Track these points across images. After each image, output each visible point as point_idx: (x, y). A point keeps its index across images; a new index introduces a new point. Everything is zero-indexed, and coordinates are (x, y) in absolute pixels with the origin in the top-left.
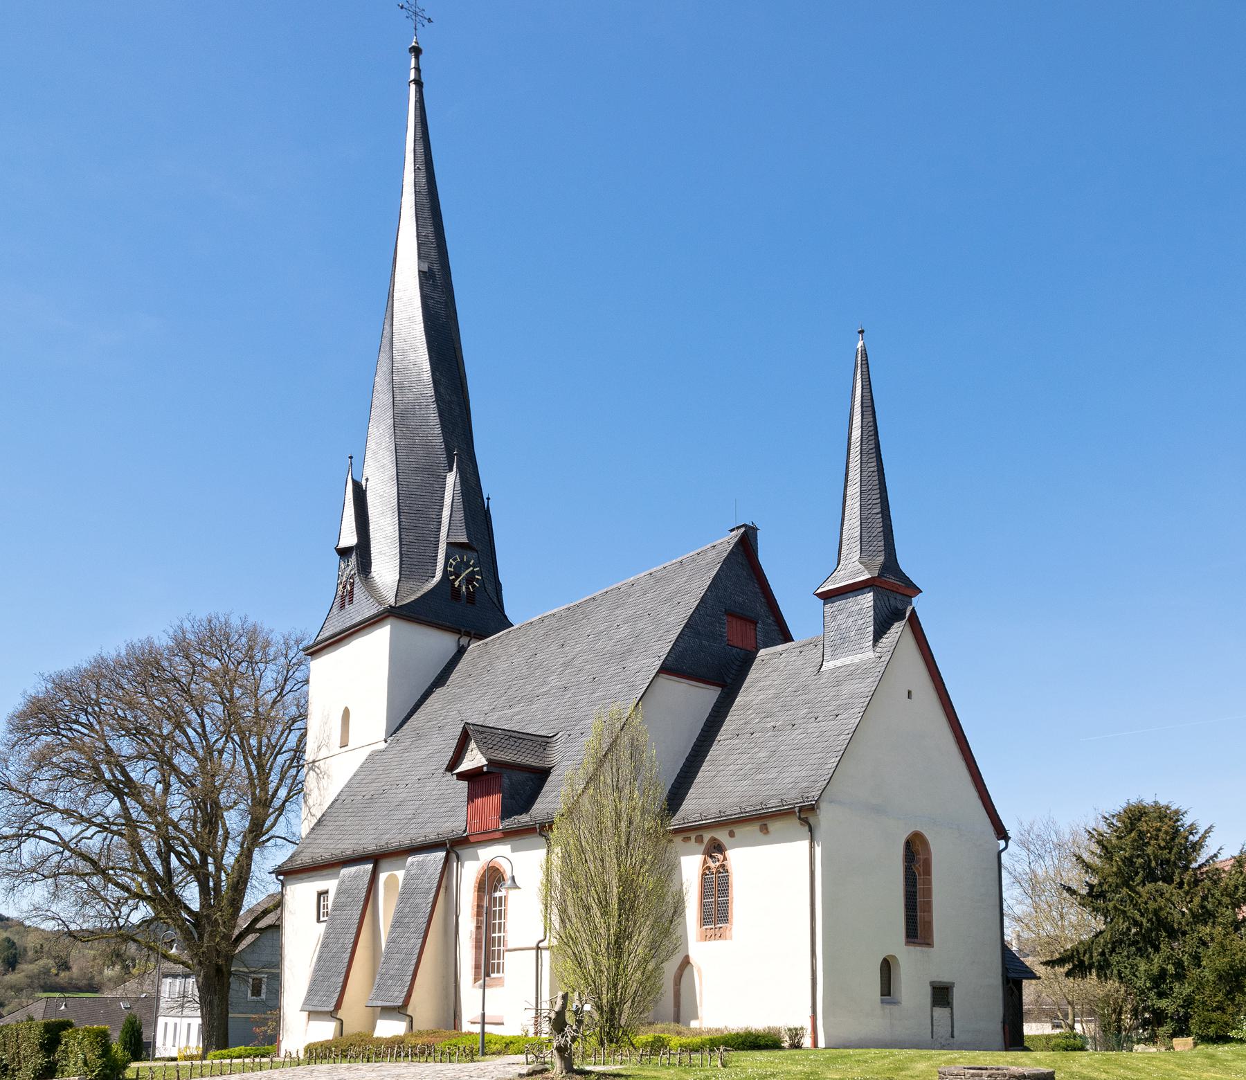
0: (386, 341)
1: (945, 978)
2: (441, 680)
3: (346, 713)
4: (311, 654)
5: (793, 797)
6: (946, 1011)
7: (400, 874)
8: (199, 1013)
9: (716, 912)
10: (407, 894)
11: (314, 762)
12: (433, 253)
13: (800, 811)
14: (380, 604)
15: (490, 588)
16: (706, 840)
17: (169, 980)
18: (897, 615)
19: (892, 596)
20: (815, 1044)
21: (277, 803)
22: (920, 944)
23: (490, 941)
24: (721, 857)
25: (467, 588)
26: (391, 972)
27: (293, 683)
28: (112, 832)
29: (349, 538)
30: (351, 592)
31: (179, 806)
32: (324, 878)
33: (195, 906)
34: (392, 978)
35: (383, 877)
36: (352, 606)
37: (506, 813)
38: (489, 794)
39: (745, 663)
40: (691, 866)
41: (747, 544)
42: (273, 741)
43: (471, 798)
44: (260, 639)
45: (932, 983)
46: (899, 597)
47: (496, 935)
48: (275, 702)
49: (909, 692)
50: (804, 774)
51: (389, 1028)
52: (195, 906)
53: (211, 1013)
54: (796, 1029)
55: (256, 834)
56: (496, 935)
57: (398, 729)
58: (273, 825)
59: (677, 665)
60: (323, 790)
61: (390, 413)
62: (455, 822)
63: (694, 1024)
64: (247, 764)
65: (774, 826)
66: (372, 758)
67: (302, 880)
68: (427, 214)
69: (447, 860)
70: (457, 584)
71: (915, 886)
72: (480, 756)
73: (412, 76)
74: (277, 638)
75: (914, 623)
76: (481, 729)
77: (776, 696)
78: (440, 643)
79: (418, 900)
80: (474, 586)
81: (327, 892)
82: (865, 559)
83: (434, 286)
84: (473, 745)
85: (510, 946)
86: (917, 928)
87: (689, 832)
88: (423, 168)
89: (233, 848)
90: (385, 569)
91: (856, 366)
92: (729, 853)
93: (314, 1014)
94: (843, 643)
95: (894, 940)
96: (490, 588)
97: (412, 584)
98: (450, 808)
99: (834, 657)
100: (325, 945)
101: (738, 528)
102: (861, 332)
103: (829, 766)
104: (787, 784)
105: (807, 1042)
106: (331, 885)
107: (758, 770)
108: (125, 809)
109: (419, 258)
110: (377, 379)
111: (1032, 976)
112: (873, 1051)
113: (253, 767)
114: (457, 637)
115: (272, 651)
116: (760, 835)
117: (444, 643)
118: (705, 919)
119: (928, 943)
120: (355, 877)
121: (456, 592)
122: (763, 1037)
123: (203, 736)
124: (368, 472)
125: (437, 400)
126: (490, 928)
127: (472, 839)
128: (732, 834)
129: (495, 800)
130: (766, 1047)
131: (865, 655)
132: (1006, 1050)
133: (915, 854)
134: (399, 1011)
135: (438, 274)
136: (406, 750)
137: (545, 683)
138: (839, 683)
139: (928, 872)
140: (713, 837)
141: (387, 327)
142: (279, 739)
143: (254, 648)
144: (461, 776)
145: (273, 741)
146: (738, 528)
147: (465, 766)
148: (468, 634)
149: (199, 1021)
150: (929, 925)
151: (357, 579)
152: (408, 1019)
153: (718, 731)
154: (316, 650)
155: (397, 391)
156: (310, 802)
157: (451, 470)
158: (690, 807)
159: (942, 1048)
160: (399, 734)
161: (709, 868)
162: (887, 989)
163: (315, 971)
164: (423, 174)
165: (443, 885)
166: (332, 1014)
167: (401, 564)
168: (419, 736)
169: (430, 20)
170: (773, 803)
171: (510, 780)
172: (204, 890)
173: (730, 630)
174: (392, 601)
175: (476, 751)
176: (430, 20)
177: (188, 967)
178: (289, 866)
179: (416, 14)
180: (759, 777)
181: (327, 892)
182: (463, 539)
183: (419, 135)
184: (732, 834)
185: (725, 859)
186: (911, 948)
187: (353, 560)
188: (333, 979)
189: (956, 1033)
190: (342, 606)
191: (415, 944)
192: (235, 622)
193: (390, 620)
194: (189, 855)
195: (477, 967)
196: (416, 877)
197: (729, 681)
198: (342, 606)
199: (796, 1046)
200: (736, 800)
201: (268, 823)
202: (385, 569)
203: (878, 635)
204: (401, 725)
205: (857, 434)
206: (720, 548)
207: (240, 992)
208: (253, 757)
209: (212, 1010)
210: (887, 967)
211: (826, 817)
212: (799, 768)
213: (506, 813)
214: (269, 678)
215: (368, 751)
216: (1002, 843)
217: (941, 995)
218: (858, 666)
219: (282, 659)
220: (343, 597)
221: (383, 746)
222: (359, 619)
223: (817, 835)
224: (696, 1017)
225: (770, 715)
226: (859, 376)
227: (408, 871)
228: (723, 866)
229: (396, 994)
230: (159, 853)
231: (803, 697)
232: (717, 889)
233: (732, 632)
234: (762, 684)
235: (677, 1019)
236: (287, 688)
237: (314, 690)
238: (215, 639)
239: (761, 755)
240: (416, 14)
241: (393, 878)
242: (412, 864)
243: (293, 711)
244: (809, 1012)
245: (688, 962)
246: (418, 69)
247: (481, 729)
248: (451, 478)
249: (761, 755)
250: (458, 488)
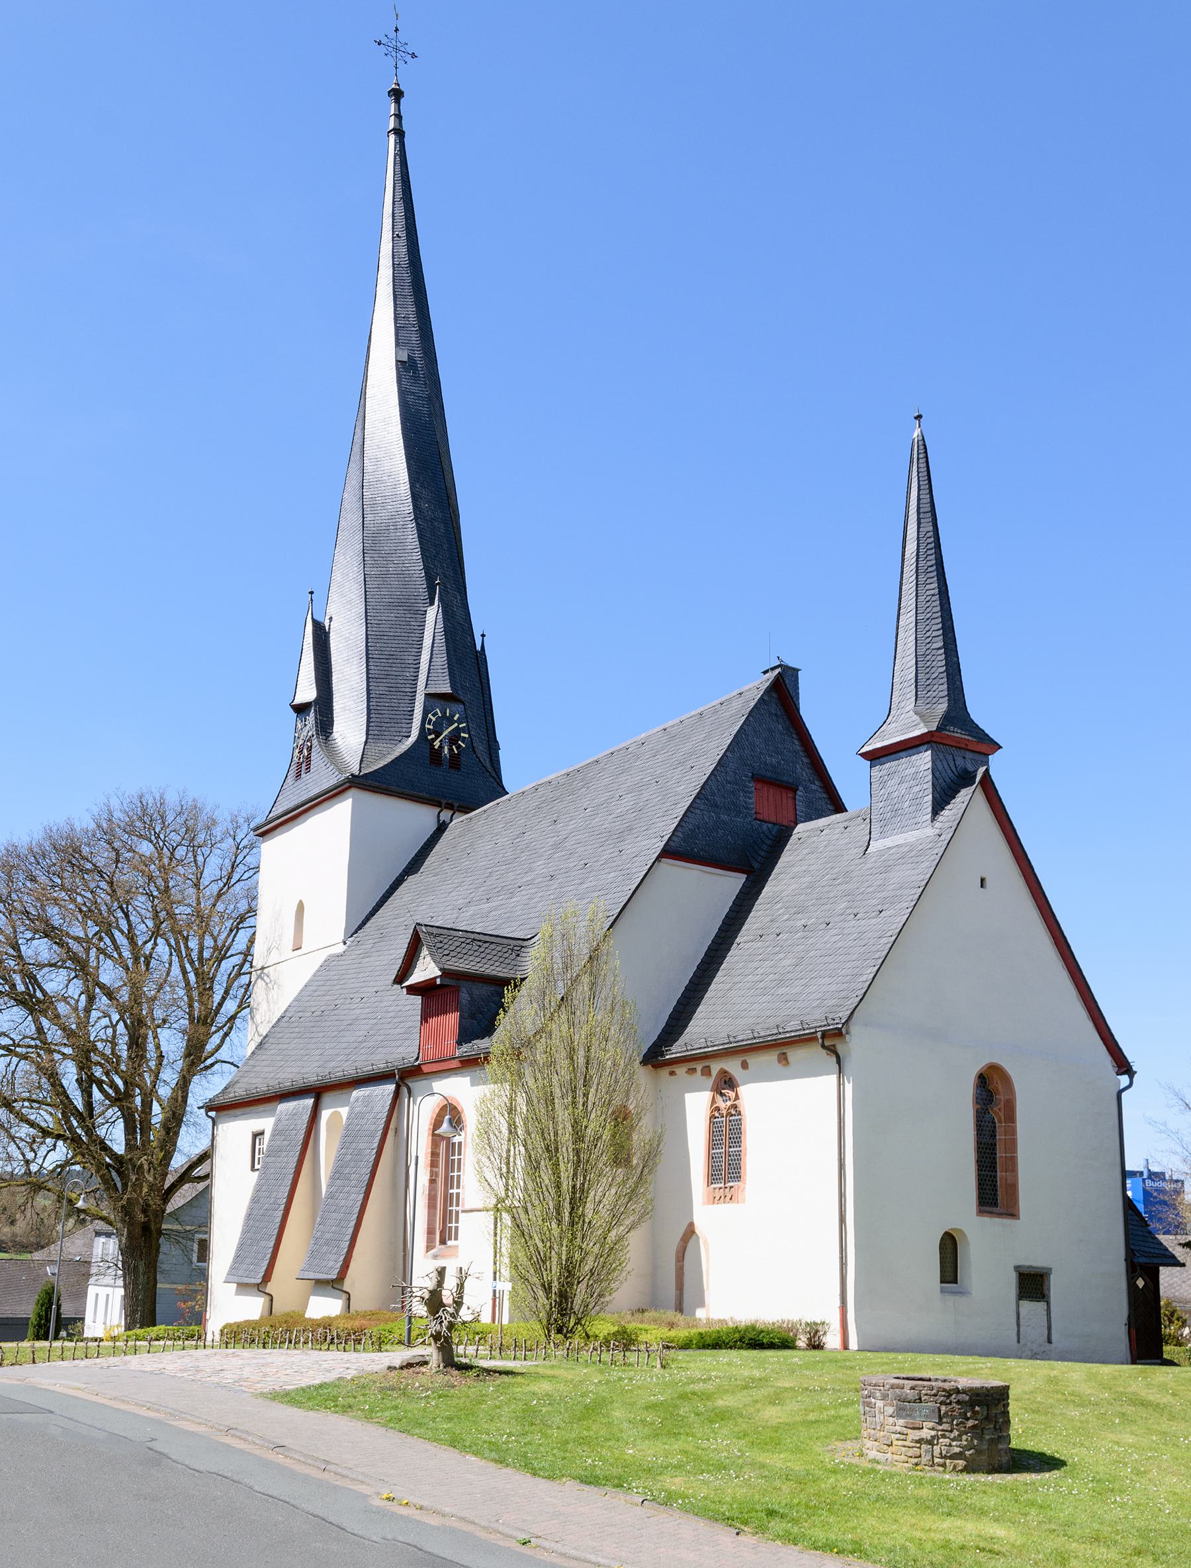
0: (357, 448)
1: (1036, 1260)
2: (414, 866)
3: (301, 907)
4: (262, 835)
5: (816, 1018)
6: (1041, 1306)
7: (344, 1111)
8: (120, 1282)
9: (726, 1168)
10: (350, 1136)
11: (263, 968)
12: (415, 338)
13: (823, 1037)
14: (340, 771)
15: (481, 748)
16: (714, 1073)
17: (102, 1239)
18: (965, 779)
19: (958, 754)
20: (845, 1346)
21: (221, 1019)
22: (1000, 1215)
23: (448, 1199)
24: (732, 1094)
25: (451, 750)
26: (327, 1236)
27: (240, 871)
28: (17, 1055)
29: (307, 692)
30: (308, 758)
31: (104, 1026)
32: (259, 1115)
33: (119, 1148)
34: (327, 1244)
35: (325, 1114)
37: (464, 1037)
38: (445, 1012)
39: (779, 840)
40: (697, 1104)
41: (782, 691)
42: (220, 943)
43: (425, 1017)
44: (203, 818)
45: (1017, 1268)
46: (969, 755)
47: (454, 1191)
48: (219, 895)
49: (982, 880)
50: (833, 988)
51: (324, 1307)
52: (119, 1148)
53: (135, 1284)
54: (815, 1324)
55: (196, 1057)
56: (454, 1191)
57: (360, 928)
58: (219, 1047)
59: (683, 848)
60: (272, 1001)
61: (359, 537)
62: (404, 1049)
63: (700, 1314)
64: (184, 972)
65: (796, 1055)
66: (329, 964)
67: (236, 1117)
68: (408, 291)
69: (397, 1094)
71: (993, 1135)
72: (433, 964)
74: (223, 817)
75: (988, 786)
76: (435, 931)
77: (811, 886)
78: (412, 819)
79: (362, 1146)
80: (459, 747)
81: (262, 1133)
82: (923, 708)
83: (415, 378)
84: (425, 951)
85: (467, 1207)
86: (994, 1191)
87: (698, 1060)
88: (403, 234)
89: (170, 1076)
90: (350, 729)
91: (911, 462)
92: (743, 1090)
93: (243, 1288)
94: (894, 818)
95: (957, 1204)
96: (481, 748)
97: (382, 746)
98: (400, 1028)
99: (883, 834)
100: (255, 1200)
101: (773, 669)
102: (919, 417)
103: (864, 978)
104: (813, 1005)
105: (832, 1340)
106: (265, 1123)
107: (781, 982)
108: (40, 1030)
109: (397, 344)
110: (346, 495)
111: (1174, 1262)
112: (926, 1356)
113: (192, 977)
115: (218, 831)
116: (779, 1067)
117: (423, 817)
118: (713, 1176)
119: (1011, 1213)
120: (294, 1114)
121: (436, 755)
122: (768, 1333)
123: (131, 938)
124: (332, 610)
125: (416, 519)
126: (450, 1182)
127: (425, 1069)
128: (745, 1065)
129: (450, 1021)
130: (771, 1346)
131: (920, 832)
132: (1133, 1362)
133: (992, 1094)
134: (334, 1284)
135: (420, 364)
136: (366, 955)
137: (531, 870)
138: (887, 869)
139: (1011, 1117)
140: (723, 1068)
141: (358, 430)
142: (227, 938)
143: (194, 832)
144: (412, 990)
145: (220, 943)
146: (773, 669)
147: (417, 977)
148: (450, 807)
149: (122, 1291)
150: (1013, 1189)
151: (315, 742)
152: (268, 1298)
153: (739, 930)
154: (266, 831)
155: (367, 509)
156: (258, 1018)
157: (432, 604)
158: (697, 1029)
159: (1034, 1356)
161: (718, 1109)
162: (950, 1272)
163: (244, 1232)
164: (403, 242)
165: (392, 1126)
166: (260, 1287)
167: (368, 722)
168: (382, 937)
169: (413, 56)
170: (792, 1027)
171: (471, 995)
172: (130, 1130)
173: (757, 797)
174: (355, 770)
175: (428, 958)
176: (413, 56)
177: (111, 1224)
178: (221, 1100)
179: (397, 49)
180: (781, 991)
181: (262, 1133)
182: (446, 689)
183: (399, 195)
184: (745, 1065)
185: (737, 1098)
186: (986, 1220)
187: (311, 717)
188: (263, 1243)
189: (1054, 1338)
190: (298, 775)
191: (355, 1201)
192: (172, 799)
193: (354, 792)
194: (113, 1085)
195: (430, 1232)
196: (361, 1116)
197: (756, 865)
198: (298, 775)
199: (815, 1345)
200: (751, 1021)
201: (209, 1047)
202: (350, 729)
203: (938, 807)
204: (364, 923)
205: (911, 547)
206: (748, 696)
207: (168, 1253)
208: (192, 963)
209: (136, 1278)
210: (950, 1246)
211: (856, 1045)
212: (829, 980)
213: (464, 1037)
214: (213, 869)
216: (1124, 1080)
217: (1032, 1284)
218: (912, 847)
219: (231, 840)
220: (299, 765)
221: (341, 948)
223: (848, 1066)
224: (702, 1304)
225: (801, 910)
226: (915, 474)
227: (352, 1109)
228: (735, 1107)
229: (331, 1263)
230: (79, 1081)
231: (843, 887)
232: (727, 1134)
233: (763, 805)
234: (796, 869)
235: (679, 1308)
236: (236, 877)
238: (147, 820)
239: (787, 962)
240: (397, 49)
241: (335, 1113)
242: (357, 1100)
243: (243, 906)
244: (838, 1303)
245: (693, 1232)
246: (398, 116)
247: (435, 931)
248: (433, 614)
249: (787, 962)
250: (440, 625)
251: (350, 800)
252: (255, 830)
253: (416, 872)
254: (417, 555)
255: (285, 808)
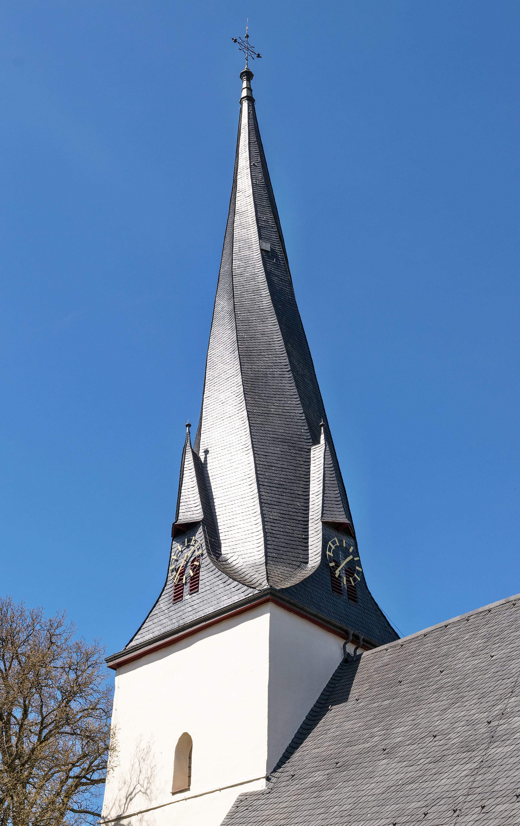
3: (185, 747)
4: (115, 667)
25: (348, 581)
29: (191, 509)
36: (195, 596)
57: (279, 766)
66: (245, 804)
70: (337, 572)
73: (244, 93)
80: (355, 580)
114: (342, 642)
121: (336, 582)
151: (206, 561)
157: (316, 442)
160: (287, 766)
169: (259, 56)
174: (265, 585)
187: (199, 536)
190: (178, 597)
193: (270, 606)
215: (234, 795)
221: (261, 785)
222: (210, 610)
237: (119, 718)
246: (249, 89)
251: (268, 615)
252: (108, 661)
253: (344, 698)
254: (296, 401)
255: (157, 633)
